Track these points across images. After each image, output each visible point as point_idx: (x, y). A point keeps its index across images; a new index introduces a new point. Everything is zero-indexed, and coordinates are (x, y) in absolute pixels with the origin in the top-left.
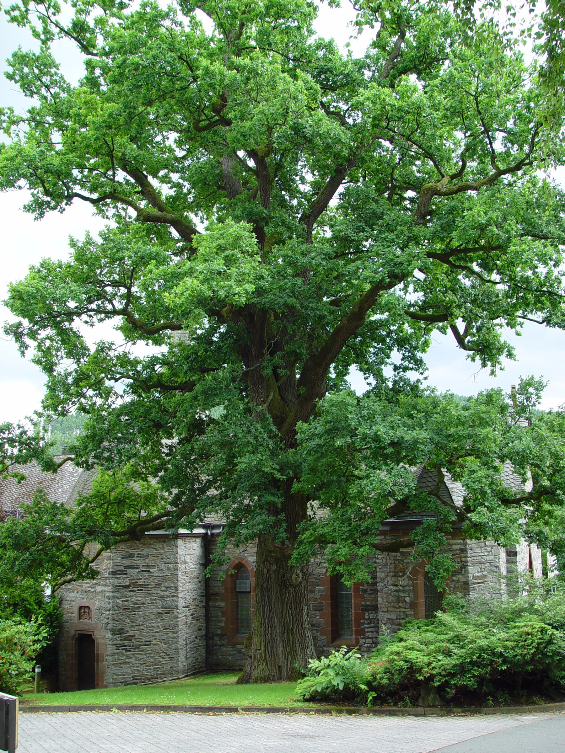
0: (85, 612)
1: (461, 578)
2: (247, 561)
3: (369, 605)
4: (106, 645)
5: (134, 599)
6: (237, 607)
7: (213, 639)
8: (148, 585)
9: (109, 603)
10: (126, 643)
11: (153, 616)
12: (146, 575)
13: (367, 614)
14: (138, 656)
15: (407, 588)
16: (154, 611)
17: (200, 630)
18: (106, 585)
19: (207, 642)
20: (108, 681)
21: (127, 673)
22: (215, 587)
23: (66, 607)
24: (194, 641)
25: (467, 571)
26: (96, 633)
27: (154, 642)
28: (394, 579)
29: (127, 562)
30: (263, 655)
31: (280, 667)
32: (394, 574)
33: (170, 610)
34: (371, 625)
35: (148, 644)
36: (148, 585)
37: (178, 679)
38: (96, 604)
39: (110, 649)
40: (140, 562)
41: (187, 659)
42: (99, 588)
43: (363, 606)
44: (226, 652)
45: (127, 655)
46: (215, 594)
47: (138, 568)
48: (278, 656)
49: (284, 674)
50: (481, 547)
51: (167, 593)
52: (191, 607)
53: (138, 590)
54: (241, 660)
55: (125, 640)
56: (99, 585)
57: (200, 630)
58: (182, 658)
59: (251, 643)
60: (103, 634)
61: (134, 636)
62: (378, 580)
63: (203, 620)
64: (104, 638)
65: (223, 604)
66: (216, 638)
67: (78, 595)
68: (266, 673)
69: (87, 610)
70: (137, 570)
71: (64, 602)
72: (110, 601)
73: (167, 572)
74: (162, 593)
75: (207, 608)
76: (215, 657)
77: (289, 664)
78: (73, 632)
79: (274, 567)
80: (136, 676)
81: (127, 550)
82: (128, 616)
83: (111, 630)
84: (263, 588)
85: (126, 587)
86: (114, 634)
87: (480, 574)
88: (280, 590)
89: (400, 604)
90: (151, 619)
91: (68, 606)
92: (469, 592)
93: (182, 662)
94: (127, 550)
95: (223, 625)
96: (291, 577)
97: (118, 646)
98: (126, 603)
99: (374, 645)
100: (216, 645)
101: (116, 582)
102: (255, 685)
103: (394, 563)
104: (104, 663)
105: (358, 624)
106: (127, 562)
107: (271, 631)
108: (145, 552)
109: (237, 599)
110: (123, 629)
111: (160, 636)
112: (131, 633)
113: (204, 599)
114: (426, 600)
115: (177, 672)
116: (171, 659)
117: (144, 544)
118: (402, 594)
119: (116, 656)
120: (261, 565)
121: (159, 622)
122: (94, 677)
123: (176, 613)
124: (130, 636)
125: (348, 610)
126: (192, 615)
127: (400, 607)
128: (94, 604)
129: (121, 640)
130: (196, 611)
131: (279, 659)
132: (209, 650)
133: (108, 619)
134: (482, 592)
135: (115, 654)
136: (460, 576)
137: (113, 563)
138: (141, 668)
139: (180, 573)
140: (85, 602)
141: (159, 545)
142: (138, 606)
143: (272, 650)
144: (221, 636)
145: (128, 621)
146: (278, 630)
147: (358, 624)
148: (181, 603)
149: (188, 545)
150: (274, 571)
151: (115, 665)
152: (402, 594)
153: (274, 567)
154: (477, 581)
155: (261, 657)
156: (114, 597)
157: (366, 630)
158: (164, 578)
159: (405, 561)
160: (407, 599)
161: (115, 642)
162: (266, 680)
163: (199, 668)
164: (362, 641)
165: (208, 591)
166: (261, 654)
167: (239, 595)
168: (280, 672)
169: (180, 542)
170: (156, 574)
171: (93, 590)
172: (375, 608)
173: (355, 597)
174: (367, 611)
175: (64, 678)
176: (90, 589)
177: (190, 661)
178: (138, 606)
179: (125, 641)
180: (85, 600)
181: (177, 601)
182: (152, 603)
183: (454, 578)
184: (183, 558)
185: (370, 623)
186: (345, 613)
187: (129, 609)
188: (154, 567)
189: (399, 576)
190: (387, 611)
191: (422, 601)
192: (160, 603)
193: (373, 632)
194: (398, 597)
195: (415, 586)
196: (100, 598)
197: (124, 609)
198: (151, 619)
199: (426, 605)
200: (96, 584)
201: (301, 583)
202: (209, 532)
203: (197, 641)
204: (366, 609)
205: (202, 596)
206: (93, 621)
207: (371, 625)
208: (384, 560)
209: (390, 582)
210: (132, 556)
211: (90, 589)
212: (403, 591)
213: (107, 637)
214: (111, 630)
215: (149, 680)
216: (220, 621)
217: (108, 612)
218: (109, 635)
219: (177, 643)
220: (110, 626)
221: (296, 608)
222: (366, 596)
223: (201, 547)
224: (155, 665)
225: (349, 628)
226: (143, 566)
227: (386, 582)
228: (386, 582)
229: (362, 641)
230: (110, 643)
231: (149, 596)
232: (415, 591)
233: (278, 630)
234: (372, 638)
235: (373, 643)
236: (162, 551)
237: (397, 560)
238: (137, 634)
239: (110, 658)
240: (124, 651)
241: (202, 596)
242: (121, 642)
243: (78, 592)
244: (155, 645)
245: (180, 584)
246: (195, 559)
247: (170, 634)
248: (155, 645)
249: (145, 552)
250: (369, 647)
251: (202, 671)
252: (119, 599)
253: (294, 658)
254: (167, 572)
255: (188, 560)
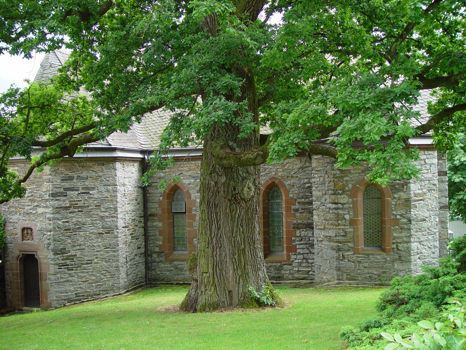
0: (27, 233)
1: (403, 195)
2: (182, 184)
3: (300, 224)
4: (48, 264)
5: (74, 220)
6: (174, 227)
7: (151, 256)
8: (88, 206)
9: (50, 224)
10: (68, 262)
11: (93, 236)
12: (86, 196)
13: (298, 232)
14: (80, 274)
15: (347, 206)
16: (95, 231)
17: (139, 248)
18: (46, 207)
19: (146, 259)
20: (51, 299)
21: (70, 290)
22: (152, 208)
23: (10, 228)
24: (134, 259)
25: (409, 189)
26: (39, 253)
27: (96, 261)
28: (333, 197)
29: (67, 185)
30: (211, 279)
31: (230, 292)
32: (333, 192)
33: (110, 230)
34: (302, 242)
35: (90, 262)
36: (88, 206)
37: (120, 294)
38: (38, 225)
39: (53, 269)
40: (79, 184)
41: (128, 275)
42: (40, 210)
43: (294, 224)
44: (163, 269)
45: (69, 274)
46: (152, 215)
47: (78, 190)
48: (228, 280)
49: (235, 300)
50: (422, 165)
51: (107, 214)
52: (131, 227)
53: (79, 211)
54: (178, 275)
55: (67, 259)
56: (40, 207)
57: (139, 248)
58: (123, 275)
59: (196, 266)
60: (46, 254)
61: (75, 255)
62: (314, 198)
63: (142, 239)
64: (46, 258)
65: (160, 224)
66: (155, 255)
67: (21, 217)
68: (215, 299)
69: (29, 232)
70: (77, 192)
71: (8, 224)
72: (51, 222)
73: (106, 194)
74: (102, 214)
75: (145, 228)
76: (154, 273)
77: (241, 289)
78: (17, 253)
79: (223, 179)
80: (79, 293)
81: (66, 172)
82: (69, 237)
83: (53, 250)
84: (209, 203)
85: (66, 208)
86: (56, 254)
87: (420, 191)
88: (230, 205)
89: (340, 222)
90: (92, 239)
91: (12, 228)
92: (410, 209)
93: (123, 278)
94: (66, 172)
95: (161, 243)
96: (242, 190)
97: (60, 266)
98: (67, 224)
99: (305, 261)
100: (155, 262)
101: (56, 204)
102: (204, 314)
103: (334, 181)
104: (48, 281)
105: (290, 241)
106: (67, 185)
107: (220, 251)
108: (84, 174)
109: (173, 220)
110: (65, 249)
111: (101, 255)
112: (73, 253)
113: (142, 220)
114: (364, 217)
115: (119, 288)
116: (113, 276)
117: (83, 167)
118: (341, 212)
119: (59, 275)
120: (208, 178)
121: (99, 242)
122: (38, 295)
123: (116, 233)
124: (71, 256)
125: (280, 227)
126: (131, 234)
127: (339, 225)
128: (36, 225)
129: (63, 260)
130: (135, 231)
131: (229, 283)
132: (148, 266)
133: (49, 239)
134: (422, 209)
135: (58, 273)
136: (402, 194)
137: (53, 185)
138: (84, 285)
139: (119, 195)
140: (27, 224)
141: (96, 168)
142: (79, 227)
143: (221, 273)
144: (159, 253)
145: (69, 241)
146: (227, 250)
147: (290, 241)
148: (121, 223)
149: (127, 169)
150: (224, 184)
151: (58, 283)
152: (341, 212)
153: (223, 179)
154: (417, 198)
155: (209, 282)
156: (54, 219)
157: (298, 247)
158: (104, 200)
159: (345, 179)
160: (347, 217)
161: (58, 262)
162: (215, 307)
163: (140, 283)
164: (293, 257)
165: (146, 215)
166: (209, 277)
167: (175, 216)
168: (231, 297)
169: (118, 165)
170: (96, 196)
171: (34, 212)
172: (310, 226)
173: (287, 216)
174: (298, 228)
175: (10, 296)
176: (31, 211)
177: (130, 277)
178: (79, 227)
179: (67, 260)
180: (27, 222)
181: (117, 222)
182: (92, 224)
183: (396, 196)
184: (121, 181)
185: (301, 240)
186: (276, 231)
187: (70, 229)
188: (93, 189)
189: (339, 194)
190: (324, 229)
191: (361, 218)
192: (100, 224)
193: (304, 249)
194: (338, 214)
195: (355, 204)
196: (41, 219)
197: (65, 230)
198: (92, 239)
199: (364, 223)
200: (37, 206)
201: (253, 197)
202: (146, 157)
203: (137, 258)
204: (297, 227)
205: (141, 217)
206: (35, 241)
207: (302, 242)
208: (322, 179)
209: (328, 200)
210: (71, 178)
211: (31, 211)
212: (342, 209)
213: (49, 257)
214: (53, 250)
215: (92, 296)
216: (157, 240)
217: (49, 233)
218: (51, 255)
219: (118, 261)
220: (52, 247)
221: (248, 225)
222: (297, 214)
223: (139, 171)
224: (97, 282)
225: (280, 245)
226: (83, 188)
227: (323, 200)
228: (323, 200)
229: (293, 257)
230: (52, 262)
231: (89, 217)
232: (355, 207)
233: (227, 250)
234: (303, 254)
235: (304, 258)
236: (101, 174)
237: (336, 178)
238: (79, 254)
239: (53, 277)
240: (66, 270)
241: (141, 217)
242: (63, 262)
243: (20, 214)
244: (96, 263)
245: (119, 205)
246: (134, 182)
247: (111, 253)
248: (96, 263)
249: (84, 174)
250: (301, 263)
251: (142, 286)
252: (59, 220)
253: (246, 281)
254: (106, 194)
255: (127, 183)
